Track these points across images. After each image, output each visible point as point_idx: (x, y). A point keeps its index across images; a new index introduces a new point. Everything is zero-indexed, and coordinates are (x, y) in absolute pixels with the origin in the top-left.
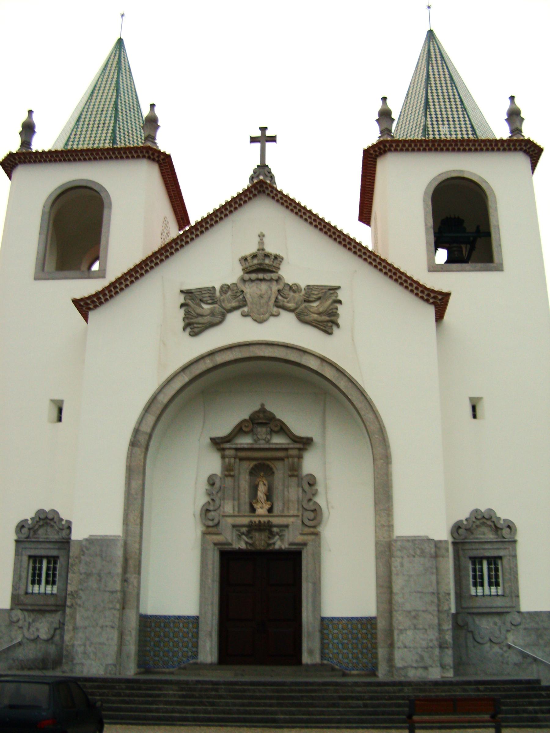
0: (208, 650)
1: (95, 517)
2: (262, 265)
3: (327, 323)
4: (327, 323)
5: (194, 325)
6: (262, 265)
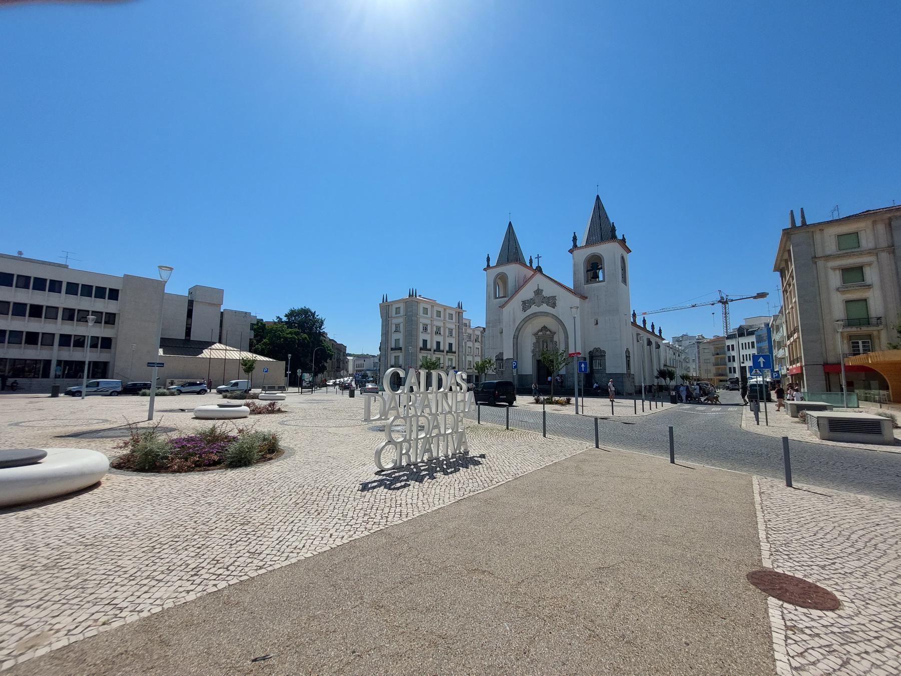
1: (508, 354)
2: (538, 292)
3: (554, 306)
4: (554, 306)
5: (524, 310)
6: (538, 292)
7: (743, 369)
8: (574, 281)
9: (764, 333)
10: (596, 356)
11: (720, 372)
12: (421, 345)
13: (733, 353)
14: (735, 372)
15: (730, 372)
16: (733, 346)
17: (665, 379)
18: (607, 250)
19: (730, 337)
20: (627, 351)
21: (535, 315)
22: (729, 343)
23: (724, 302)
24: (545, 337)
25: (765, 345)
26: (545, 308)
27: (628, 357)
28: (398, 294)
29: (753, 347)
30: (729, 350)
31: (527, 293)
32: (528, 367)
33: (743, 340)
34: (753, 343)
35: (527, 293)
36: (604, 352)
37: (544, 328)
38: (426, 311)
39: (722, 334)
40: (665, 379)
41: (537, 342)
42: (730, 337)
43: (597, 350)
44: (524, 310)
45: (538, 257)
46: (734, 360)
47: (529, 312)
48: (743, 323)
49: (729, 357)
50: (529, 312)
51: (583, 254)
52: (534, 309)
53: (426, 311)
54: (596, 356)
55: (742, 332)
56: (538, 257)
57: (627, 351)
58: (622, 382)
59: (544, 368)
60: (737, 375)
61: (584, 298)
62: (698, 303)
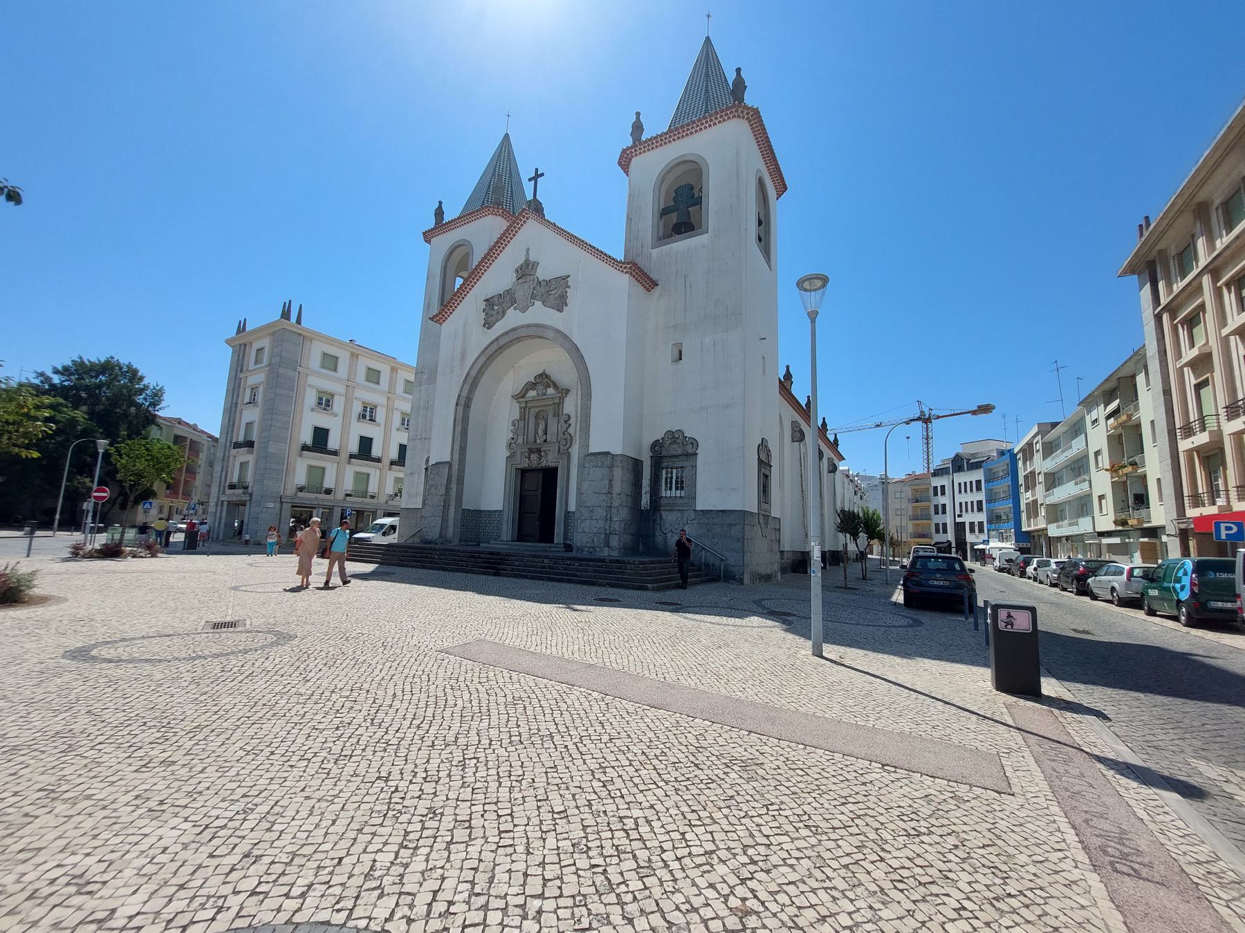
0: (506, 530)
2: (526, 270)
3: (560, 304)
4: (560, 304)
6: (526, 270)
7: (960, 528)
8: (628, 240)
9: (1001, 466)
10: (670, 457)
11: (920, 530)
12: (307, 437)
13: (942, 500)
14: (945, 531)
15: (937, 531)
16: (943, 487)
17: (855, 536)
18: (721, 147)
19: (938, 473)
20: (763, 446)
21: (514, 338)
22: (937, 482)
23: (926, 420)
24: (544, 402)
25: (1003, 486)
26: (539, 313)
27: (764, 464)
28: (264, 315)
29: (979, 489)
30: (936, 494)
31: (498, 278)
32: (492, 491)
33: (961, 478)
34: (978, 482)
35: (498, 278)
36: (694, 443)
37: (544, 379)
38: (330, 362)
39: (920, 470)
40: (855, 536)
41: (523, 417)
42: (938, 473)
43: (675, 437)
44: (488, 325)
45: (537, 176)
46: (944, 512)
47: (500, 327)
48: (960, 450)
49: (936, 506)
50: (500, 327)
51: (652, 164)
52: (513, 318)
53: (330, 362)
54: (670, 457)
55: (958, 464)
56: (537, 176)
57: (763, 446)
58: (742, 539)
59: (538, 489)
60: (950, 536)
61: (647, 281)
62: (886, 421)
